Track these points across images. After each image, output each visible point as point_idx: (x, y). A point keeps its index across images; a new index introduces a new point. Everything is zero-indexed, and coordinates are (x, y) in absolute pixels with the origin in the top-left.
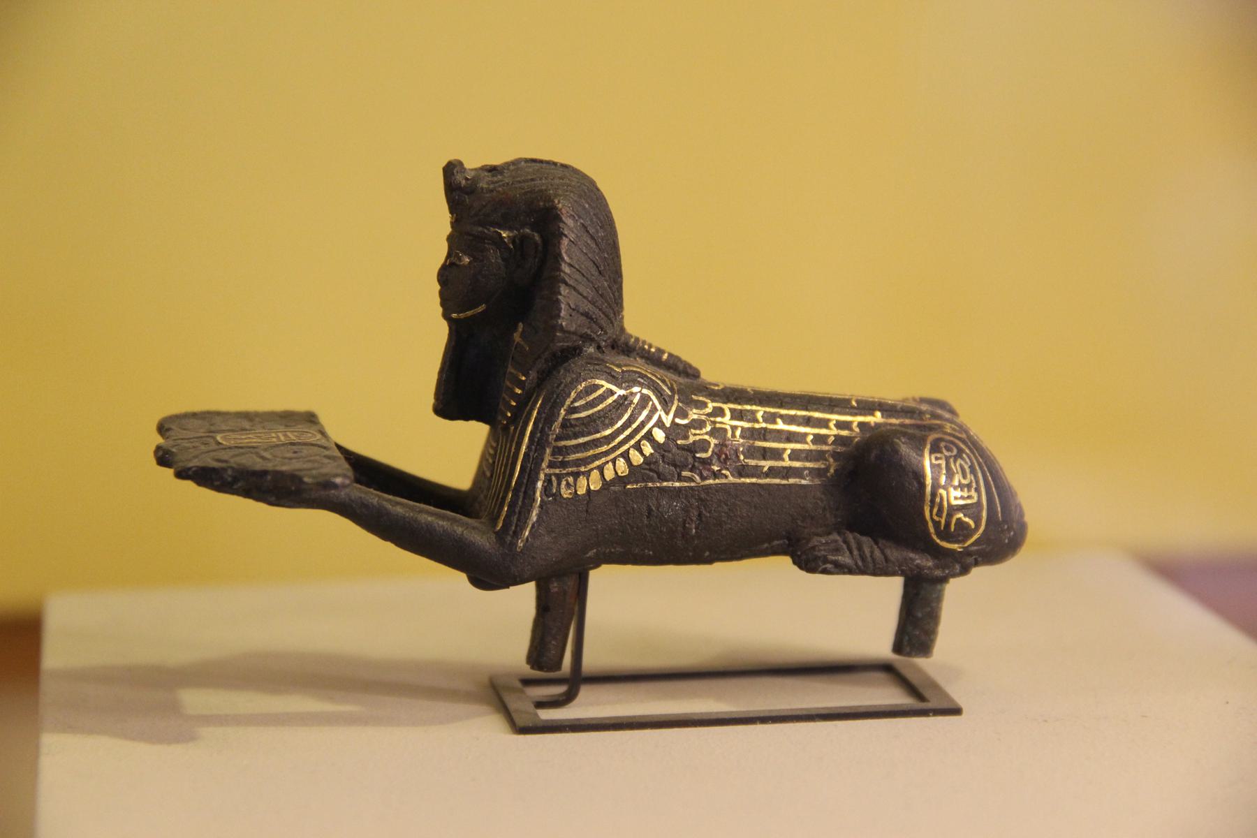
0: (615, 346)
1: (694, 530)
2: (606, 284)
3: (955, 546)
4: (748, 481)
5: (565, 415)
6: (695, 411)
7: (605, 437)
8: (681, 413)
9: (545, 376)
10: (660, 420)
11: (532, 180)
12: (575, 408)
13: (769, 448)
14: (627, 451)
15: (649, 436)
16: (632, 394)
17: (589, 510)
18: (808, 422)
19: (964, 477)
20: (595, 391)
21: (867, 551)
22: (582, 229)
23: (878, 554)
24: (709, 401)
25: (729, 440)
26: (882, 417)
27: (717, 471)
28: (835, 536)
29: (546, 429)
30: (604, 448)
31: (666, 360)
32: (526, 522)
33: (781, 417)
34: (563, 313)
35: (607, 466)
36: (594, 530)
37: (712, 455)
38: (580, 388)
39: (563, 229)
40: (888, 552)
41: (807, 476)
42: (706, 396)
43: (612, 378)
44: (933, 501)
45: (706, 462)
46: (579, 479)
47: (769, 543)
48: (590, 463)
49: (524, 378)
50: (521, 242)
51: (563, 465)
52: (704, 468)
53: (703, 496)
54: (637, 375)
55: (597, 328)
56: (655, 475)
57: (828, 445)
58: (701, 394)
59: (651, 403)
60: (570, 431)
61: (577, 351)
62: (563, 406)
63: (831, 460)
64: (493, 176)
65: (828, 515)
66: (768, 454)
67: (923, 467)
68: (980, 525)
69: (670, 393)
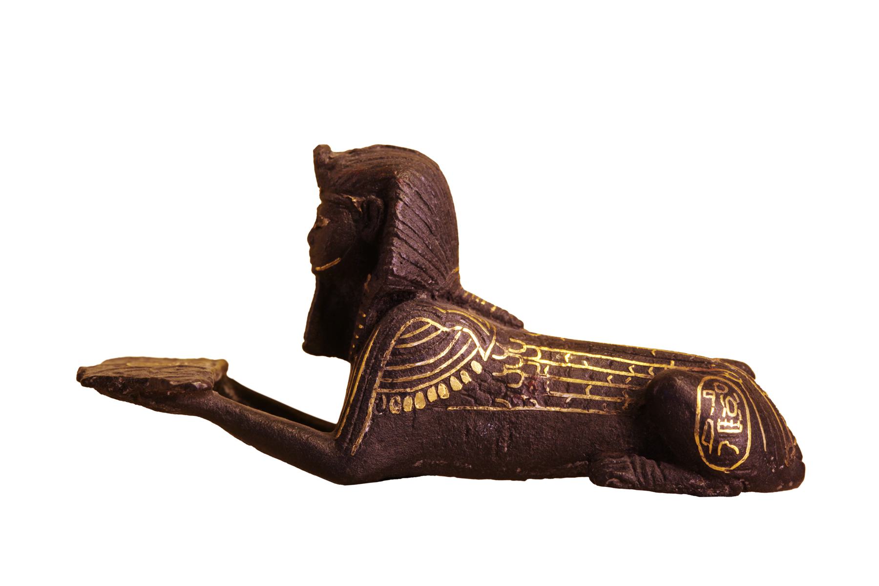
0: (450, 298)
1: (506, 449)
2: (437, 243)
3: (723, 469)
4: (553, 409)
5: (395, 345)
6: (510, 350)
7: (429, 365)
8: (498, 351)
9: (382, 314)
10: (478, 354)
11: (381, 158)
12: (404, 339)
13: (572, 383)
14: (448, 378)
15: (468, 367)
16: (454, 331)
17: (415, 426)
18: (611, 365)
19: (732, 410)
20: (421, 327)
21: (649, 470)
22: (417, 196)
23: (657, 473)
24: (524, 343)
25: (538, 374)
26: (675, 365)
27: (526, 399)
28: (626, 459)
29: (379, 356)
30: (428, 374)
31: (494, 312)
32: (359, 432)
33: (587, 359)
34: (394, 260)
35: (430, 389)
37: (522, 386)
38: (408, 323)
39: (399, 194)
40: (667, 472)
41: (605, 408)
42: (522, 340)
43: (438, 317)
44: (702, 428)
45: (517, 392)
46: (405, 399)
47: (573, 464)
48: (415, 386)
49: (364, 316)
50: (368, 206)
51: (392, 386)
52: (515, 397)
53: (513, 419)
54: (459, 317)
55: (427, 278)
57: (626, 384)
58: (517, 338)
59: (470, 340)
60: (398, 358)
61: (411, 296)
62: (394, 338)
63: (627, 396)
64: (352, 156)
65: (621, 441)
66: (571, 388)
67: (695, 399)
68: (745, 453)
69: (489, 334)
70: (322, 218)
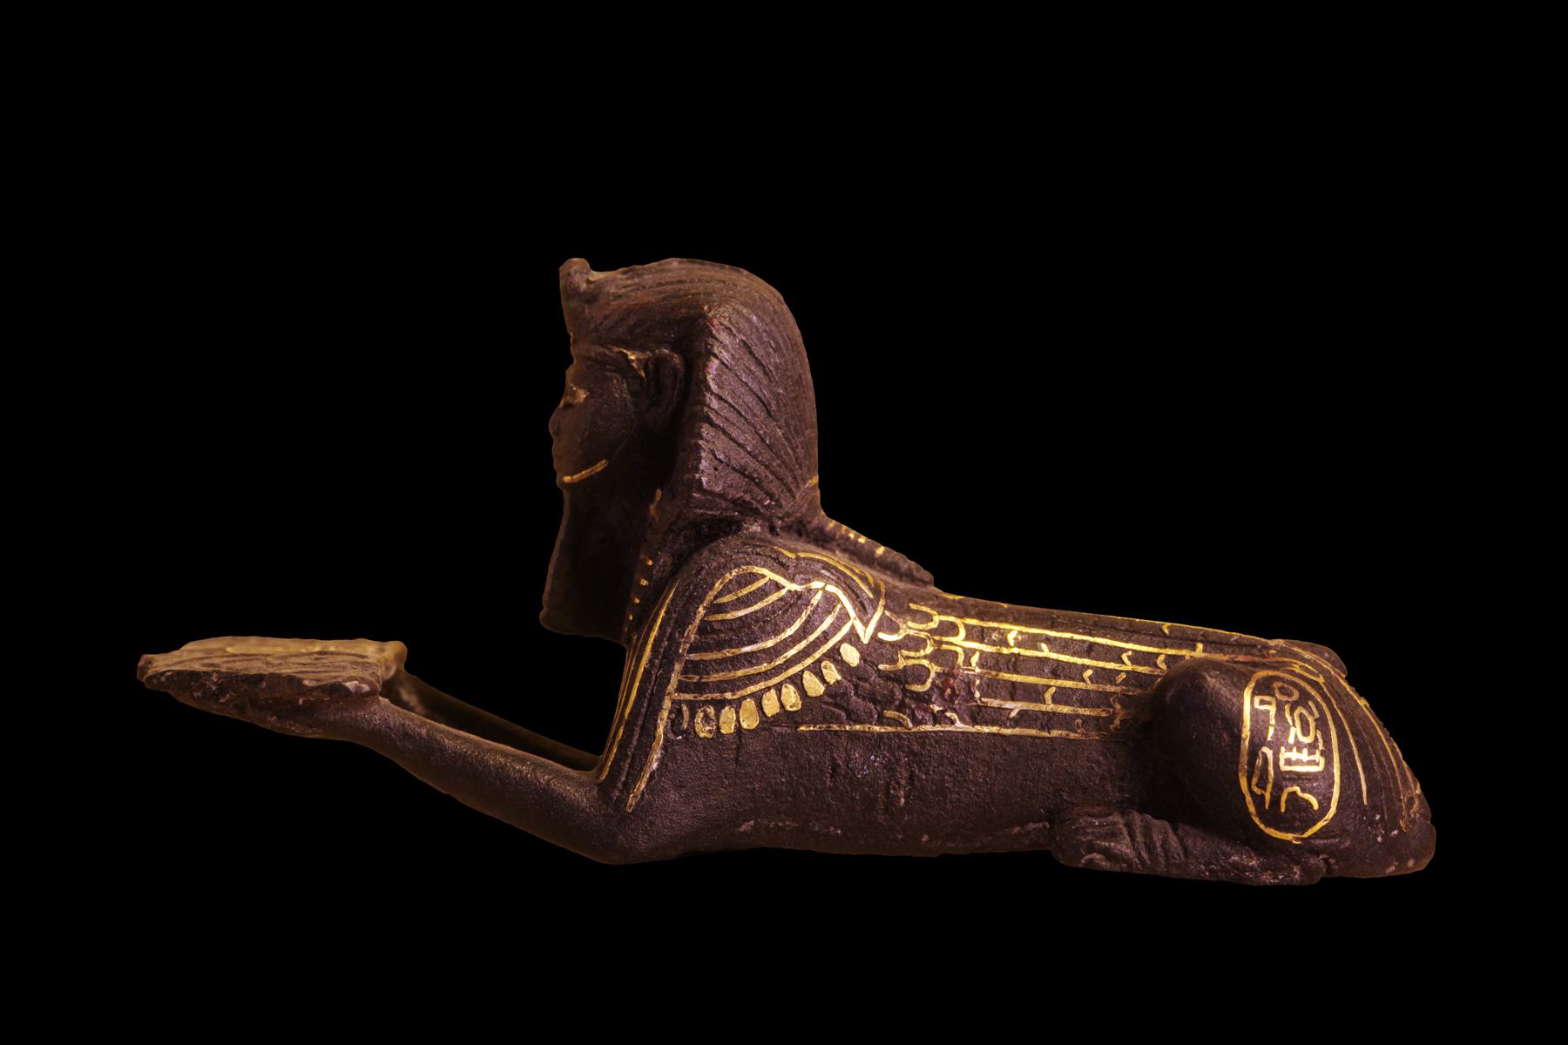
0: (803, 531)
1: (903, 800)
2: (780, 432)
3: (1289, 837)
4: (986, 729)
5: (705, 615)
6: (910, 624)
7: (765, 651)
8: (887, 625)
9: (681, 561)
10: (853, 631)
11: (680, 282)
12: (720, 605)
13: (1021, 683)
14: (800, 675)
15: (834, 655)
16: (809, 590)
17: (741, 759)
18: (1090, 650)
19: (1306, 732)
20: (751, 583)
21: (1157, 839)
22: (743, 349)
24: (935, 613)
25: (959, 667)
27: (938, 711)
28: (1116, 818)
29: (677, 635)
30: (764, 667)
32: (641, 770)
33: (1048, 640)
34: (704, 464)
35: (768, 693)
36: (747, 789)
37: (931, 688)
38: (728, 577)
39: (712, 346)
40: (1189, 842)
41: (1079, 728)
42: (932, 607)
43: (781, 566)
44: (1251, 763)
45: (922, 698)
46: (723, 711)
47: (1022, 827)
48: (740, 688)
49: (650, 563)
50: (657, 367)
51: (700, 688)
52: (919, 708)
53: (916, 748)
54: (820, 565)
55: (761, 495)
56: (843, 714)
57: (1116, 685)
58: (922, 603)
59: (839, 606)
60: (711, 638)
61: (734, 528)
62: (702, 603)
63: (1118, 706)
64: (628, 279)
65: (1109, 787)
66: (1019, 692)
67: (1241, 711)
68: (1329, 807)
69: (872, 596)
70: (575, 389)
